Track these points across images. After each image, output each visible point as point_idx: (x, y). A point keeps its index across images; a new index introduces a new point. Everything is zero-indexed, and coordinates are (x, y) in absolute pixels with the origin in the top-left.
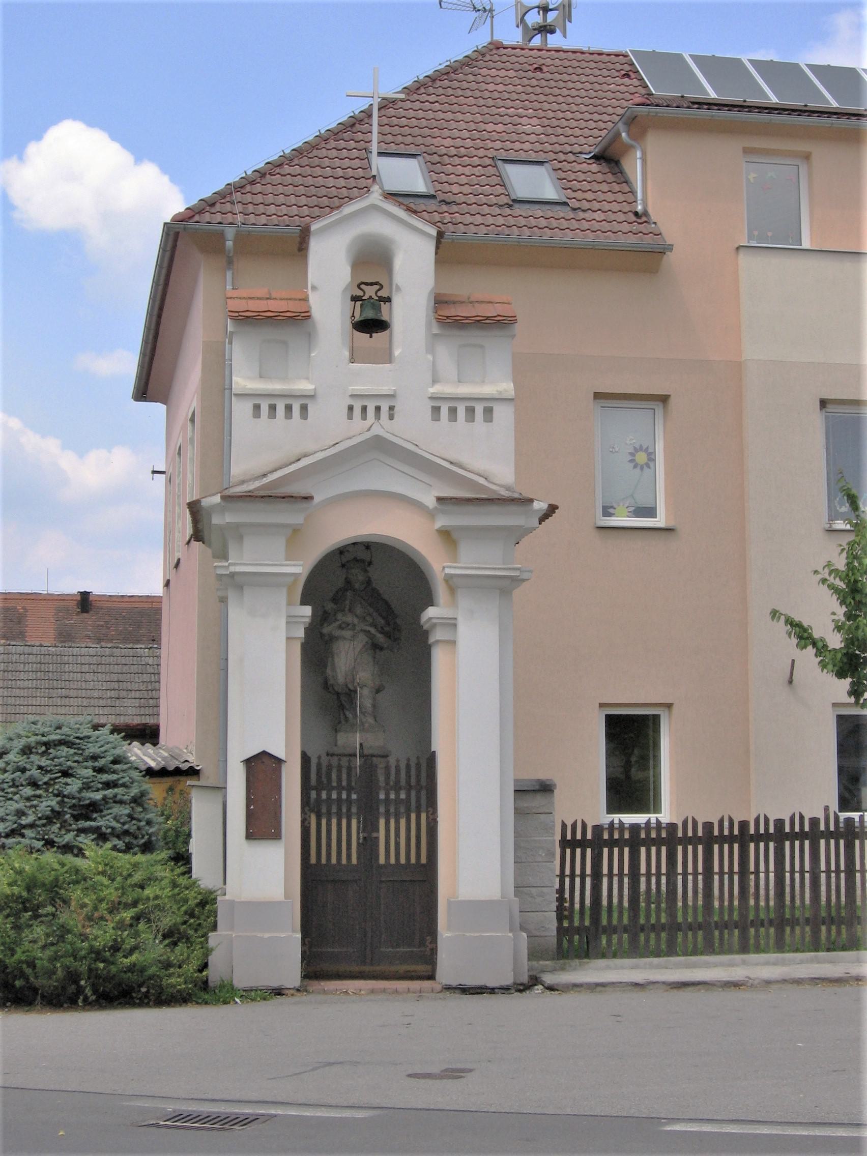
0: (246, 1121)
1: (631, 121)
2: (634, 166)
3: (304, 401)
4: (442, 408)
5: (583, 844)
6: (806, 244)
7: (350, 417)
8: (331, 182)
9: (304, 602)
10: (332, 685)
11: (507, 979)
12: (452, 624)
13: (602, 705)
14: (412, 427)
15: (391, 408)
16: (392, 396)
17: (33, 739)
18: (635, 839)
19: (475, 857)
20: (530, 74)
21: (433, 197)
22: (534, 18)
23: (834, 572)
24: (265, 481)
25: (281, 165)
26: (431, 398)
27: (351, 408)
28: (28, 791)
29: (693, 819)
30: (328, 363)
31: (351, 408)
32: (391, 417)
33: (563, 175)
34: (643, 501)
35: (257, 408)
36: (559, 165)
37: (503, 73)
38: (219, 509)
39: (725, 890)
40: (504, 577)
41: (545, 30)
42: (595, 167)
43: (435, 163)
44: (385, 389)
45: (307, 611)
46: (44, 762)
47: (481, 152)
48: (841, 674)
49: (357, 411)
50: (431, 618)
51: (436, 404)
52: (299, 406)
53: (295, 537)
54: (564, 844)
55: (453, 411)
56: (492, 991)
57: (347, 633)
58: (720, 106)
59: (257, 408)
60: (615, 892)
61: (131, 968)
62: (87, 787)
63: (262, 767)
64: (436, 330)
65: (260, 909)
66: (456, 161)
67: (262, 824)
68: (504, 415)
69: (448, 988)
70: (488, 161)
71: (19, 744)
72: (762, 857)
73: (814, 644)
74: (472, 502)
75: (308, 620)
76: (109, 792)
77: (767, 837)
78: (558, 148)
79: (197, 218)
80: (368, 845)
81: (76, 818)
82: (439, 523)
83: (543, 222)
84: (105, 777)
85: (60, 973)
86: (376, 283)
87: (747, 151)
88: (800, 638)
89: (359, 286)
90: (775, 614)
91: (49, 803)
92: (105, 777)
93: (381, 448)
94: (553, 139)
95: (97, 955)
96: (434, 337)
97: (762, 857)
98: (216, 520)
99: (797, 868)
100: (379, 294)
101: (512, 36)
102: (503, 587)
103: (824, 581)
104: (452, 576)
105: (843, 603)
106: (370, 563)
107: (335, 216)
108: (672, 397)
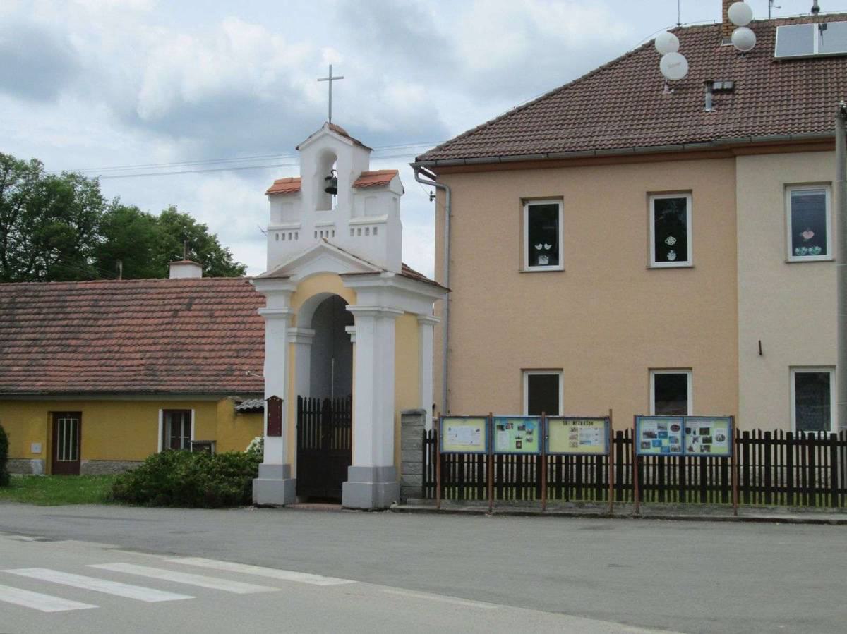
3: (375, 226)
4: (356, 230)
7: (316, 237)
13: (791, 367)
14: (342, 238)
16: (333, 226)
18: (812, 442)
19: (371, 444)
26: (350, 225)
27: (316, 232)
31: (316, 232)
32: (333, 236)
40: (372, 311)
44: (330, 222)
49: (319, 234)
51: (353, 228)
54: (425, 441)
60: (757, 469)
99: (757, 463)
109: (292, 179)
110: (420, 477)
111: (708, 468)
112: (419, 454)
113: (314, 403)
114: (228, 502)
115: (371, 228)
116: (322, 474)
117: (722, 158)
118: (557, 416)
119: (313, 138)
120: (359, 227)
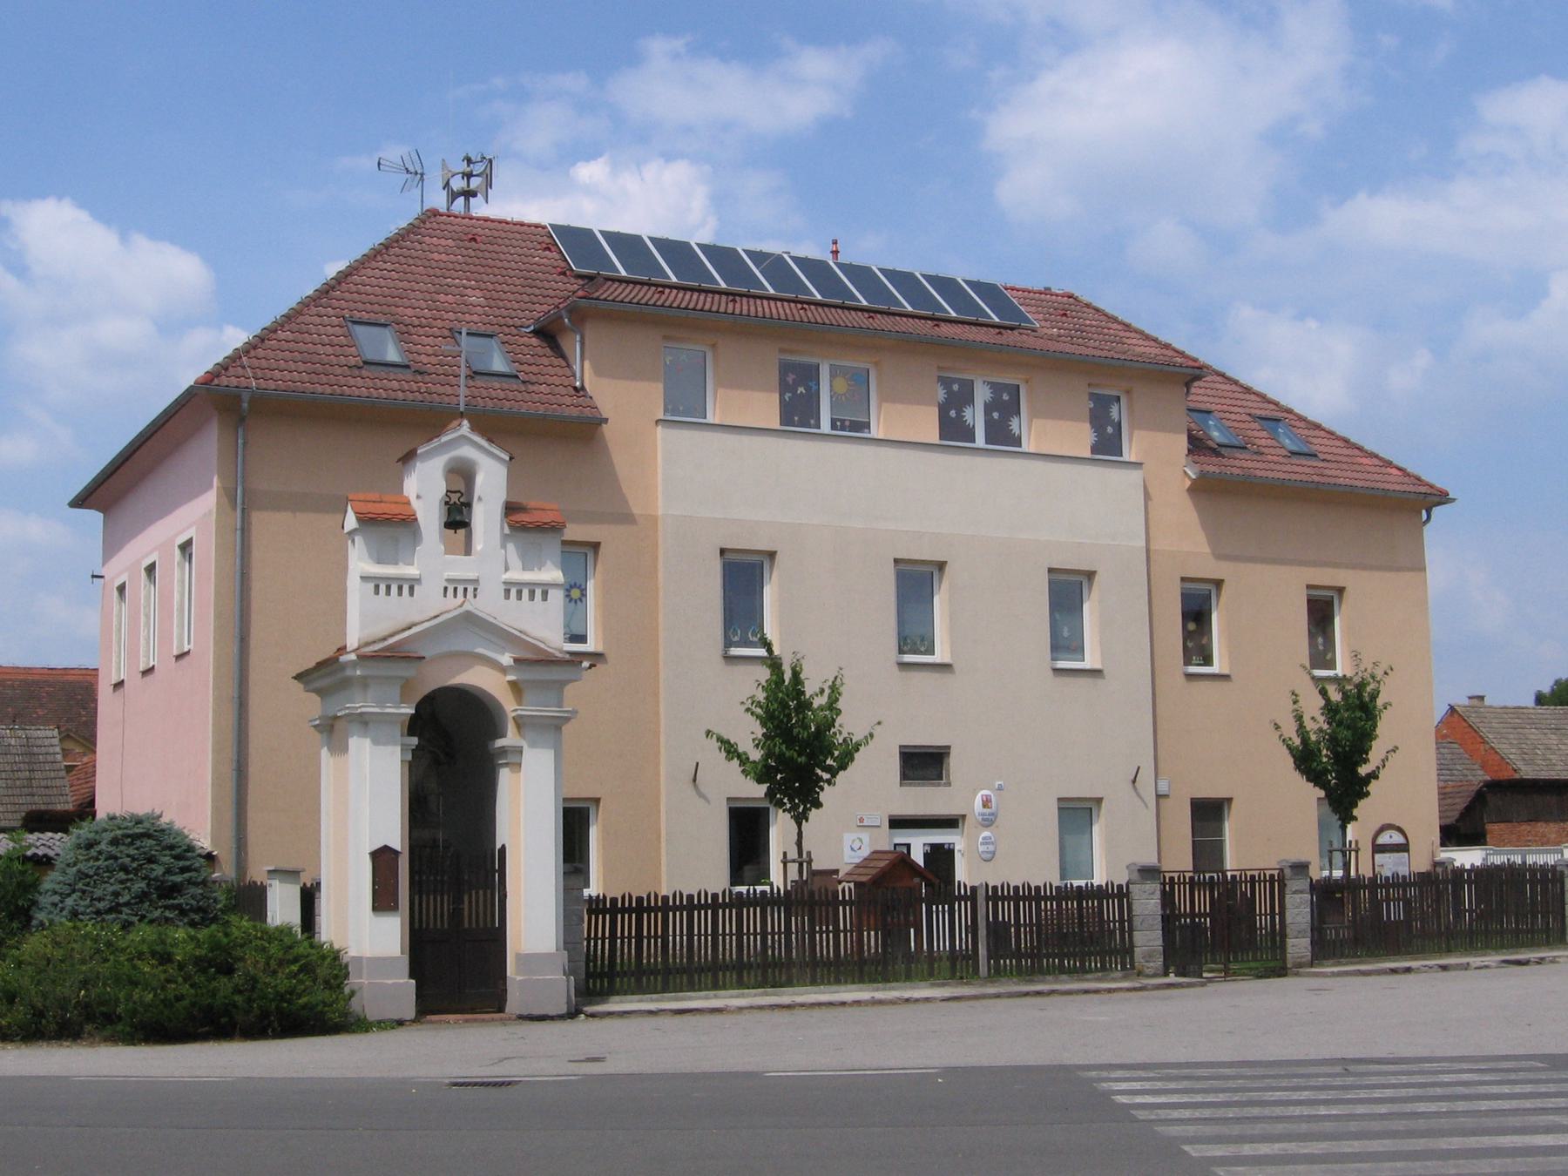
0: (509, 1083)
1: (573, 311)
2: (573, 345)
4: (513, 589)
5: (604, 911)
6: (710, 419)
8: (321, 349)
11: (563, 1009)
12: (519, 751)
14: (489, 604)
16: (476, 581)
17: (119, 832)
19: (533, 919)
20: (467, 244)
21: (407, 367)
22: (458, 184)
23: (759, 705)
24: (386, 643)
25: (275, 331)
28: (122, 875)
30: (431, 558)
33: (510, 348)
34: (577, 631)
35: (377, 587)
36: (506, 338)
37: (443, 242)
39: (650, 949)
41: (469, 194)
42: (534, 341)
43: (404, 334)
44: (472, 575)
46: (132, 852)
47: (439, 323)
48: (760, 781)
52: (409, 585)
55: (519, 593)
56: (552, 1018)
58: (627, 282)
59: (377, 587)
61: (304, 1007)
62: (168, 871)
65: (380, 963)
66: (421, 331)
67: (383, 900)
68: (557, 596)
69: (521, 1018)
70: (447, 333)
71: (108, 836)
72: (677, 921)
73: (739, 756)
74: (537, 663)
76: (186, 875)
77: (1009, 898)
78: (502, 321)
79: (216, 381)
80: (456, 914)
81: (160, 897)
82: (511, 678)
83: (502, 395)
84: (181, 863)
85: (256, 1011)
87: (665, 338)
88: (728, 752)
90: (708, 733)
91: (140, 886)
92: (181, 863)
93: (470, 620)
94: (497, 312)
95: (281, 997)
96: (505, 539)
97: (650, 923)
101: (438, 200)
102: (553, 727)
103: (748, 710)
104: (521, 716)
105: (763, 724)
107: (435, 443)
108: (1129, 861)
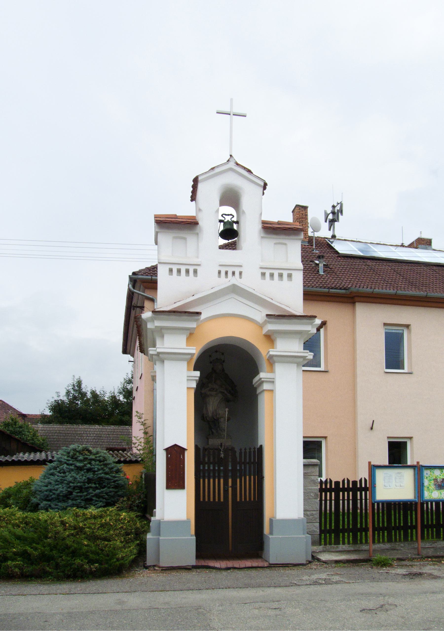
9: (195, 369)
10: (206, 417)
14: (251, 281)
15: (241, 273)
19: (286, 496)
27: (219, 272)
29: (347, 479)
31: (219, 272)
32: (241, 277)
35: (171, 270)
38: (152, 320)
45: (198, 374)
49: (223, 274)
50: (261, 379)
51: (264, 271)
52: (192, 270)
53: (191, 335)
54: (321, 490)
57: (214, 393)
59: (171, 270)
63: (175, 453)
64: (263, 235)
75: (198, 378)
86: (231, 215)
89: (222, 216)
93: (235, 290)
96: (262, 237)
98: (150, 326)
100: (233, 219)
106: (224, 361)
109: (176, 215)
110: (318, 524)
111: (341, 502)
112: (316, 502)
113: (245, 453)
114: (108, 567)
115: (285, 273)
116: (231, 531)
117: (343, 302)
118: (405, 465)
119: (217, 170)
120: (272, 271)
